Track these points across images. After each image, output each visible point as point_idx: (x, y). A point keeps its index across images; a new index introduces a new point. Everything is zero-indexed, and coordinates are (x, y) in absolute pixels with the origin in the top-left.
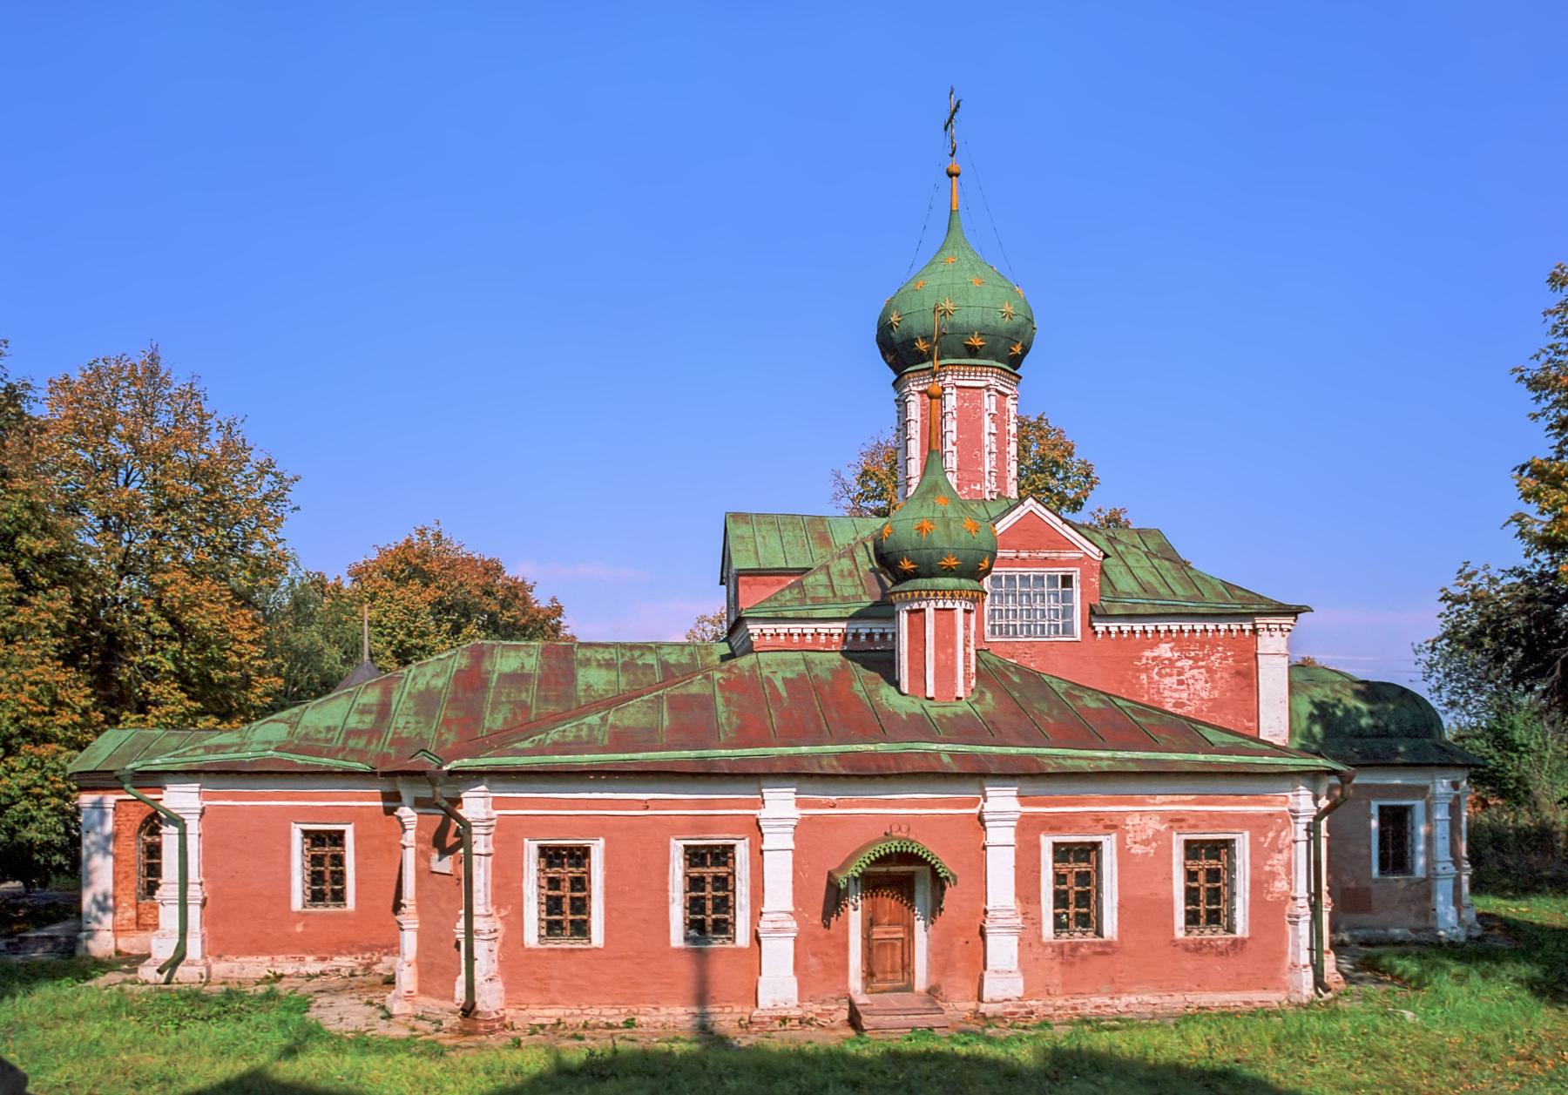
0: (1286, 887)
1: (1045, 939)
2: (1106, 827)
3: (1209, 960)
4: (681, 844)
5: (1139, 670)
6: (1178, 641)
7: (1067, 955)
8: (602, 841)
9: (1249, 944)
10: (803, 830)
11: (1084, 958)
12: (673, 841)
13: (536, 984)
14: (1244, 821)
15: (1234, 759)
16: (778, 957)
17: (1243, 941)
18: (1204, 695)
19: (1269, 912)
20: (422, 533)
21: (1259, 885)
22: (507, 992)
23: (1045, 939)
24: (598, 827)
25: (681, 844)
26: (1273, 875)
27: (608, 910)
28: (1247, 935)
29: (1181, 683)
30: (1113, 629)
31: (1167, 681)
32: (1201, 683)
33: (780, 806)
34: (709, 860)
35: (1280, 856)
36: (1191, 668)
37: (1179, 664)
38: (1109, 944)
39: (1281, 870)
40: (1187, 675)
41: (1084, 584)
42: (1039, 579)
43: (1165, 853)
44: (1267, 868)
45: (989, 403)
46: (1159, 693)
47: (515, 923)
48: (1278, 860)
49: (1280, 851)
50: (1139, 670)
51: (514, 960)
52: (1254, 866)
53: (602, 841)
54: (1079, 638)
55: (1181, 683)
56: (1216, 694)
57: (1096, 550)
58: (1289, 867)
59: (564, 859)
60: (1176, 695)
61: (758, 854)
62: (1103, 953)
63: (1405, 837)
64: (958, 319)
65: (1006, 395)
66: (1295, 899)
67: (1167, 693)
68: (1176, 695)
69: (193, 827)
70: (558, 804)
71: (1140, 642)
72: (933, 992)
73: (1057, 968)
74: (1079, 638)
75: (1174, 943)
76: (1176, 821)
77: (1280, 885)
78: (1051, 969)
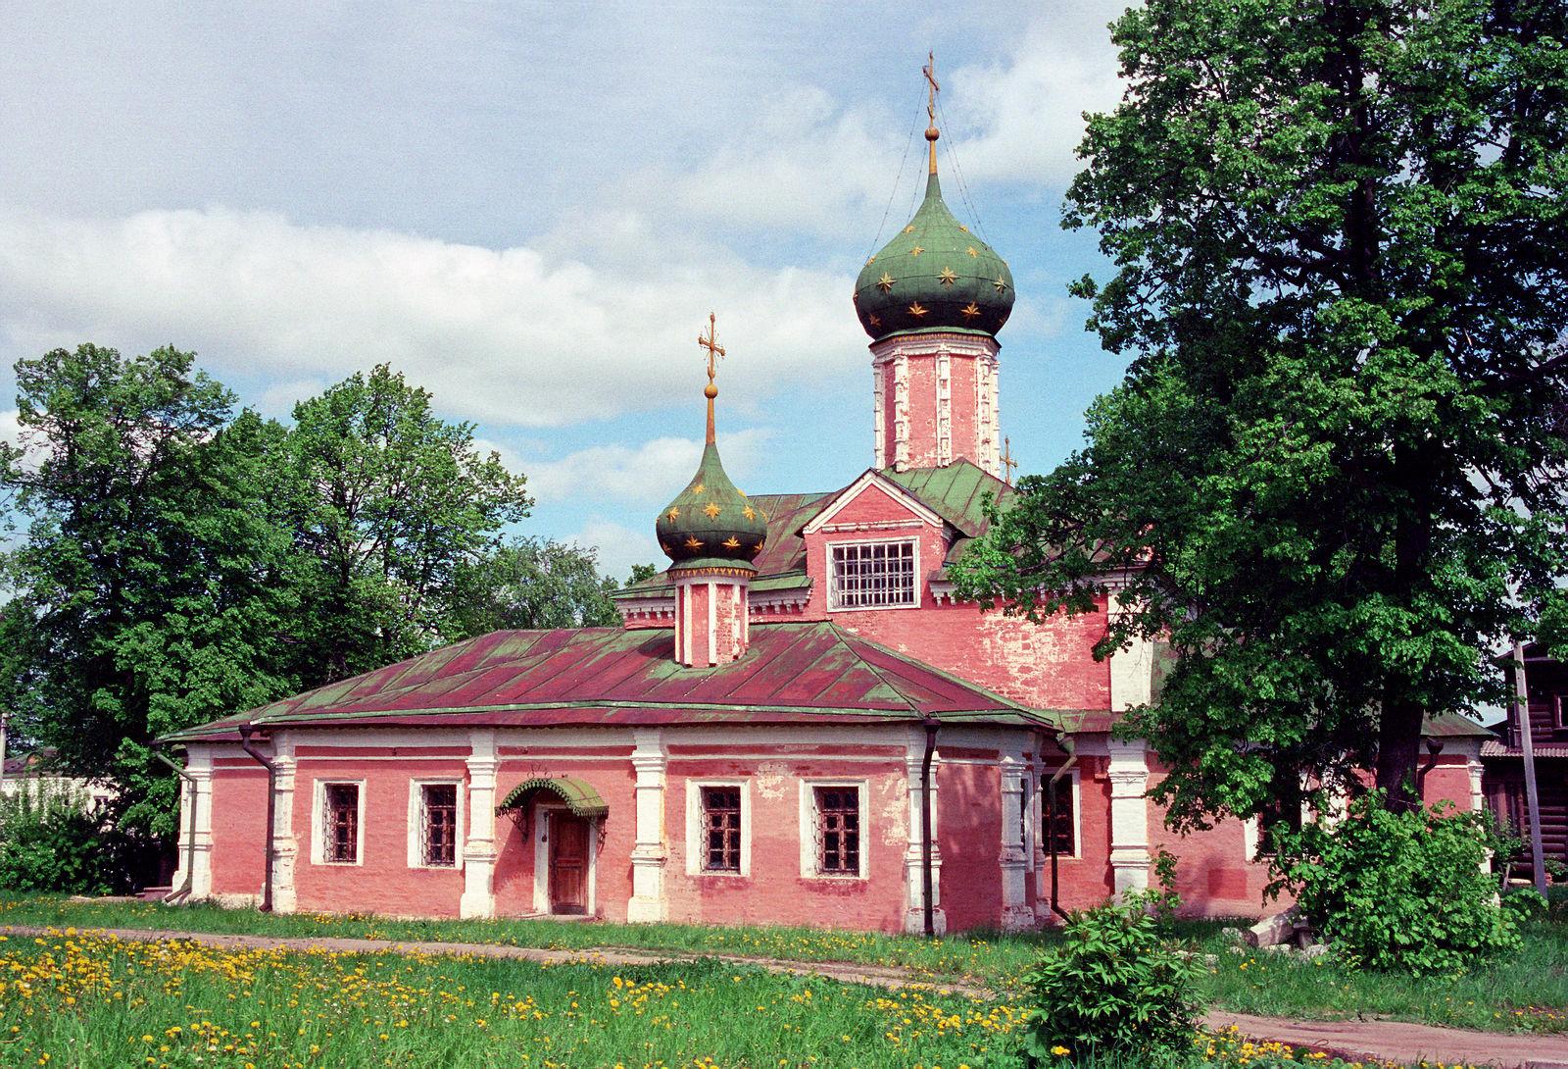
0: (904, 833)
1: (689, 872)
2: (741, 773)
3: (833, 898)
4: (419, 784)
5: (982, 635)
7: (706, 886)
9: (871, 887)
11: (721, 891)
12: (412, 781)
13: (317, 894)
15: (319, 716)
16: (479, 875)
17: (864, 883)
18: (1053, 659)
20: (1264, 286)
22: (299, 899)
23: (689, 872)
25: (419, 784)
26: (891, 822)
28: (867, 878)
29: (1026, 647)
31: (1012, 645)
32: (1050, 647)
35: (897, 804)
36: (1038, 631)
37: (1023, 627)
38: (743, 879)
39: (898, 816)
40: (1033, 639)
41: (924, 551)
42: (879, 551)
44: (885, 815)
46: (1003, 657)
47: (305, 846)
49: (898, 799)
50: (982, 635)
51: (305, 874)
52: (873, 813)
55: (1026, 647)
56: (1066, 657)
57: (935, 518)
58: (906, 812)
60: (1022, 660)
62: (739, 888)
64: (894, 291)
65: (972, 358)
66: (909, 845)
67: (1011, 658)
68: (1022, 660)
70: (848, 781)
72: (599, 911)
73: (699, 898)
75: (800, 882)
77: (897, 832)
78: (692, 899)
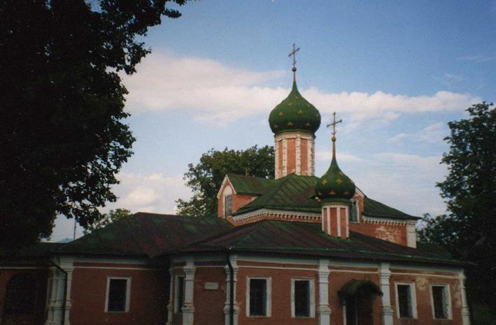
6: (385, 225)
8: (270, 278)
10: (331, 276)
14: (448, 281)
19: (457, 311)
21: (454, 302)
24: (271, 273)
26: (457, 299)
27: (273, 303)
28: (452, 319)
30: (378, 221)
33: (324, 269)
34: (302, 289)
43: (427, 289)
45: (298, 143)
48: (458, 293)
52: (452, 296)
53: (270, 278)
54: (359, 222)
58: (461, 296)
59: (258, 287)
61: (317, 284)
63: (441, 299)
69: (70, 277)
71: (376, 225)
74: (359, 222)
76: (430, 279)
